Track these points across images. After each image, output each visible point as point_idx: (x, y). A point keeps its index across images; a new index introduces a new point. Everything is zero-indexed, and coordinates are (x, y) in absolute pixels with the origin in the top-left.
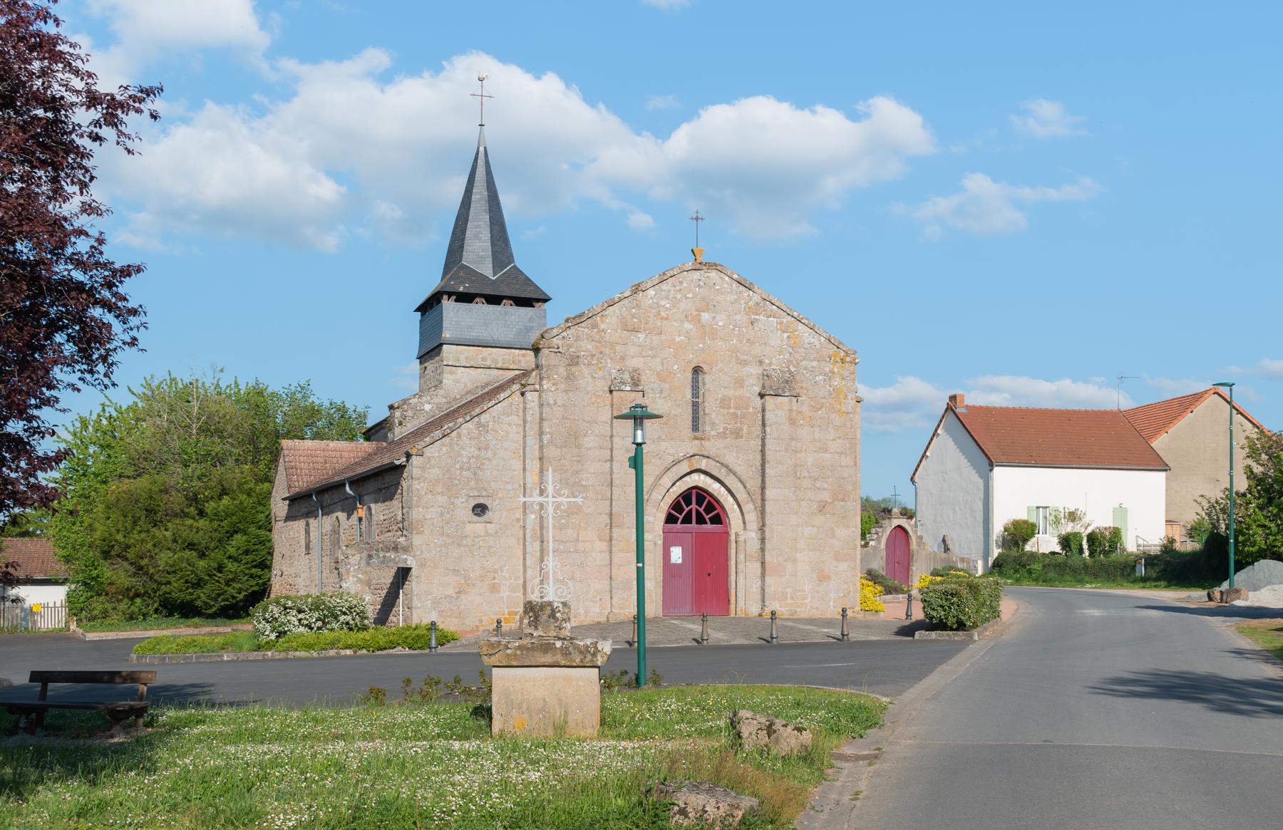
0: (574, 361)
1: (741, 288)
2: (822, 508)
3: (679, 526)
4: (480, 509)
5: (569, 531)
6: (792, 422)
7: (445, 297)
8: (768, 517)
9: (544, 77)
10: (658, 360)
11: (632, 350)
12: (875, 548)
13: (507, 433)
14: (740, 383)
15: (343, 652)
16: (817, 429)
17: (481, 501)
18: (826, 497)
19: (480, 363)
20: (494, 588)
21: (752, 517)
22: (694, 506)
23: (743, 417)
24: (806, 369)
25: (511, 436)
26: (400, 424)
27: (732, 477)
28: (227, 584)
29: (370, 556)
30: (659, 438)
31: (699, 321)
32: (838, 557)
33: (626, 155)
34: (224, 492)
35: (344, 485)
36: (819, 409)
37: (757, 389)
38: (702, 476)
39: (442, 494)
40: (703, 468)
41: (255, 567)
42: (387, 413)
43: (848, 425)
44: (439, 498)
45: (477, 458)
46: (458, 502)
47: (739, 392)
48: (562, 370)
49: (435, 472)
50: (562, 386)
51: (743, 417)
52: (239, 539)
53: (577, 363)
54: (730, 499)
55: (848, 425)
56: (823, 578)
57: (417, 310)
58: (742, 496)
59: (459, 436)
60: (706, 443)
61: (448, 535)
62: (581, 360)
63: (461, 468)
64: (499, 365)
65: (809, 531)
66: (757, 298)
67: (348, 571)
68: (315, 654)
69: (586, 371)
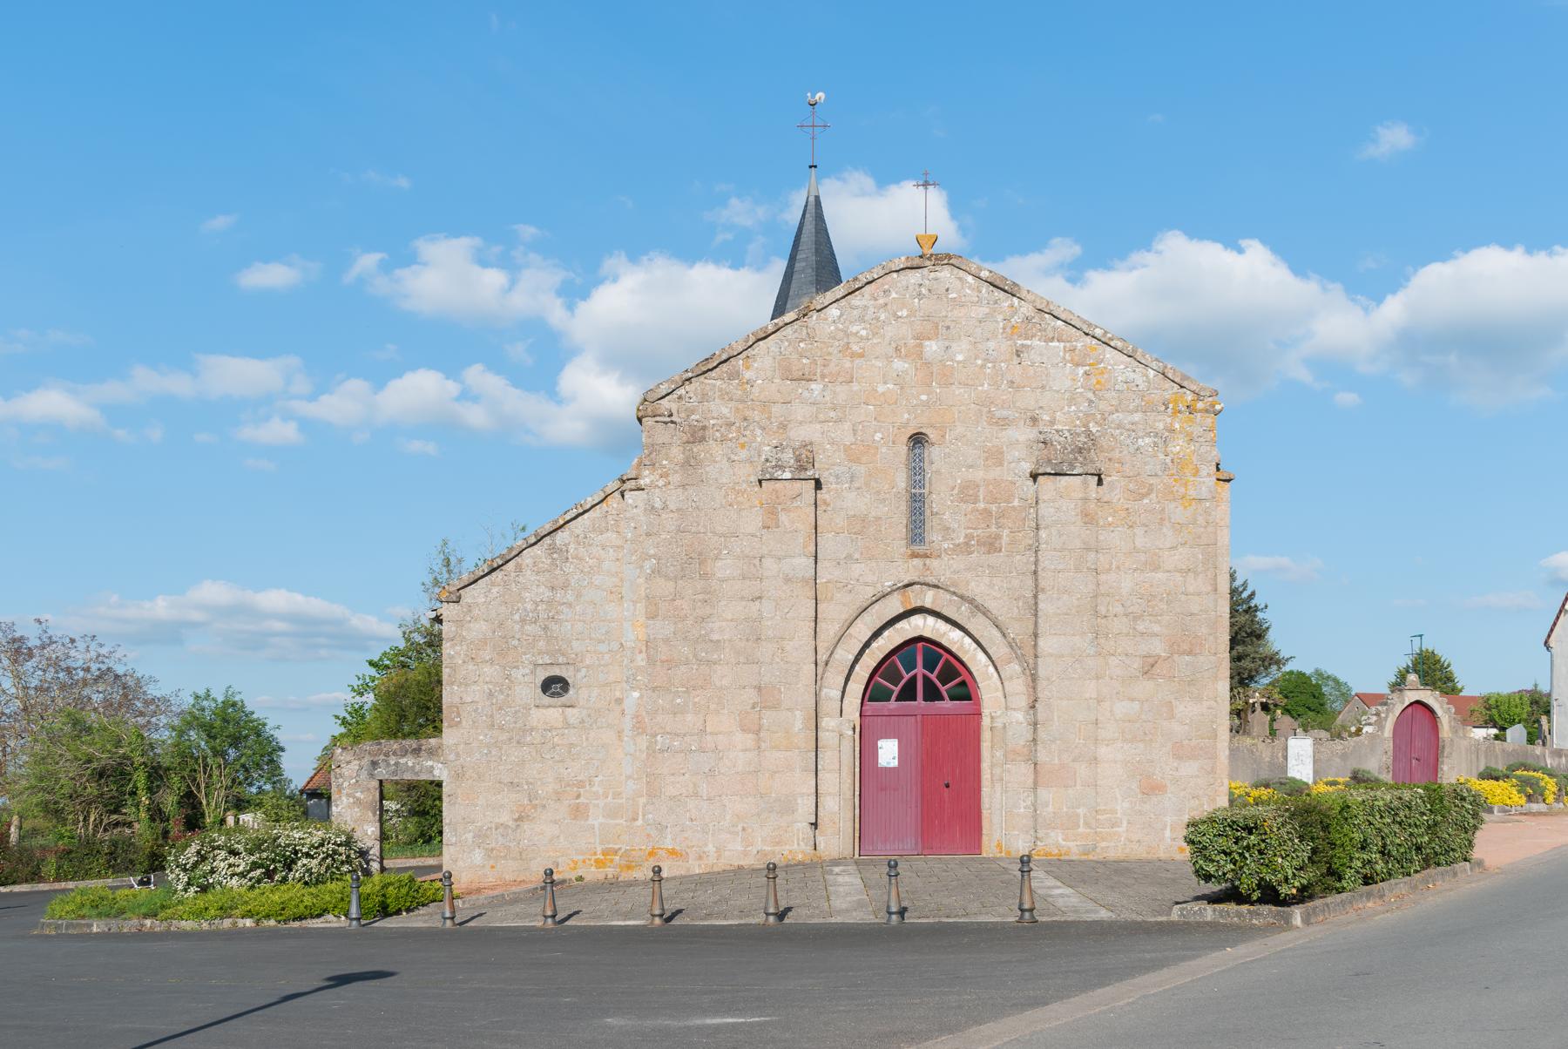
0: (698, 435)
1: (997, 293)
2: (1150, 667)
3: (893, 704)
4: (554, 685)
5: (689, 717)
6: (1088, 519)
8: (1042, 684)
10: (847, 426)
11: (800, 411)
12: (1372, 736)
13: (600, 561)
14: (995, 456)
15: (241, 923)
16: (1139, 531)
17: (556, 672)
18: (1158, 648)
20: (578, 812)
21: (1018, 686)
22: (920, 670)
23: (1002, 515)
24: (1119, 426)
25: (606, 565)
27: (980, 618)
29: (374, 764)
30: (849, 557)
31: (920, 355)
32: (1180, 753)
33: (1343, 325)
36: (1144, 496)
37: (1027, 467)
38: (931, 620)
39: (492, 662)
40: (928, 605)
43: (1201, 520)
44: (487, 669)
45: (550, 602)
46: (517, 674)
47: (995, 473)
48: (677, 453)
49: (478, 629)
50: (676, 478)
51: (1002, 515)
53: (703, 439)
54: (981, 656)
55: (1201, 520)
56: (1152, 789)
58: (999, 649)
59: (519, 569)
60: (934, 563)
61: (501, 728)
62: (708, 433)
63: (523, 621)
65: (1122, 708)
66: (1026, 309)
67: (340, 788)
68: (205, 925)
69: (717, 450)
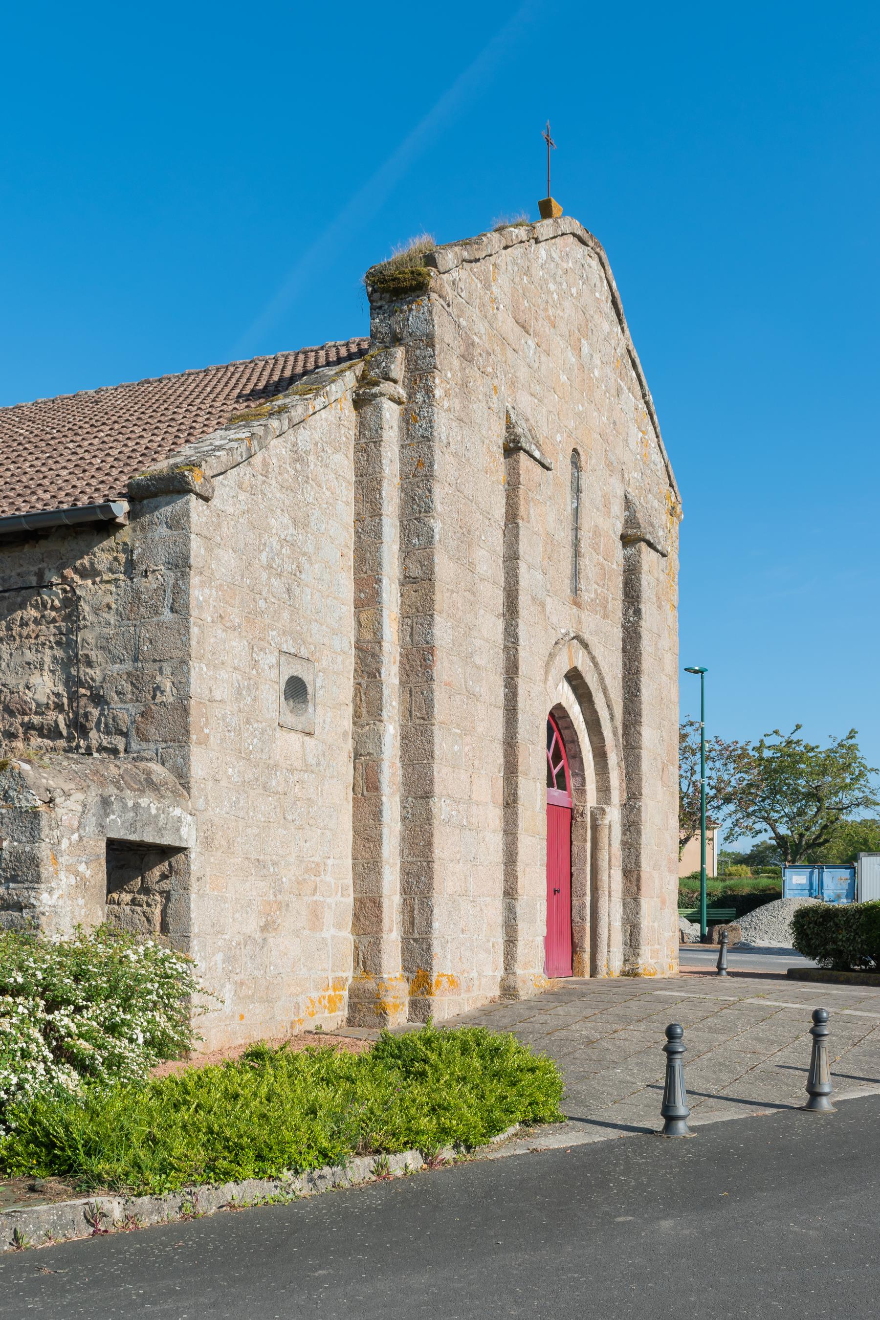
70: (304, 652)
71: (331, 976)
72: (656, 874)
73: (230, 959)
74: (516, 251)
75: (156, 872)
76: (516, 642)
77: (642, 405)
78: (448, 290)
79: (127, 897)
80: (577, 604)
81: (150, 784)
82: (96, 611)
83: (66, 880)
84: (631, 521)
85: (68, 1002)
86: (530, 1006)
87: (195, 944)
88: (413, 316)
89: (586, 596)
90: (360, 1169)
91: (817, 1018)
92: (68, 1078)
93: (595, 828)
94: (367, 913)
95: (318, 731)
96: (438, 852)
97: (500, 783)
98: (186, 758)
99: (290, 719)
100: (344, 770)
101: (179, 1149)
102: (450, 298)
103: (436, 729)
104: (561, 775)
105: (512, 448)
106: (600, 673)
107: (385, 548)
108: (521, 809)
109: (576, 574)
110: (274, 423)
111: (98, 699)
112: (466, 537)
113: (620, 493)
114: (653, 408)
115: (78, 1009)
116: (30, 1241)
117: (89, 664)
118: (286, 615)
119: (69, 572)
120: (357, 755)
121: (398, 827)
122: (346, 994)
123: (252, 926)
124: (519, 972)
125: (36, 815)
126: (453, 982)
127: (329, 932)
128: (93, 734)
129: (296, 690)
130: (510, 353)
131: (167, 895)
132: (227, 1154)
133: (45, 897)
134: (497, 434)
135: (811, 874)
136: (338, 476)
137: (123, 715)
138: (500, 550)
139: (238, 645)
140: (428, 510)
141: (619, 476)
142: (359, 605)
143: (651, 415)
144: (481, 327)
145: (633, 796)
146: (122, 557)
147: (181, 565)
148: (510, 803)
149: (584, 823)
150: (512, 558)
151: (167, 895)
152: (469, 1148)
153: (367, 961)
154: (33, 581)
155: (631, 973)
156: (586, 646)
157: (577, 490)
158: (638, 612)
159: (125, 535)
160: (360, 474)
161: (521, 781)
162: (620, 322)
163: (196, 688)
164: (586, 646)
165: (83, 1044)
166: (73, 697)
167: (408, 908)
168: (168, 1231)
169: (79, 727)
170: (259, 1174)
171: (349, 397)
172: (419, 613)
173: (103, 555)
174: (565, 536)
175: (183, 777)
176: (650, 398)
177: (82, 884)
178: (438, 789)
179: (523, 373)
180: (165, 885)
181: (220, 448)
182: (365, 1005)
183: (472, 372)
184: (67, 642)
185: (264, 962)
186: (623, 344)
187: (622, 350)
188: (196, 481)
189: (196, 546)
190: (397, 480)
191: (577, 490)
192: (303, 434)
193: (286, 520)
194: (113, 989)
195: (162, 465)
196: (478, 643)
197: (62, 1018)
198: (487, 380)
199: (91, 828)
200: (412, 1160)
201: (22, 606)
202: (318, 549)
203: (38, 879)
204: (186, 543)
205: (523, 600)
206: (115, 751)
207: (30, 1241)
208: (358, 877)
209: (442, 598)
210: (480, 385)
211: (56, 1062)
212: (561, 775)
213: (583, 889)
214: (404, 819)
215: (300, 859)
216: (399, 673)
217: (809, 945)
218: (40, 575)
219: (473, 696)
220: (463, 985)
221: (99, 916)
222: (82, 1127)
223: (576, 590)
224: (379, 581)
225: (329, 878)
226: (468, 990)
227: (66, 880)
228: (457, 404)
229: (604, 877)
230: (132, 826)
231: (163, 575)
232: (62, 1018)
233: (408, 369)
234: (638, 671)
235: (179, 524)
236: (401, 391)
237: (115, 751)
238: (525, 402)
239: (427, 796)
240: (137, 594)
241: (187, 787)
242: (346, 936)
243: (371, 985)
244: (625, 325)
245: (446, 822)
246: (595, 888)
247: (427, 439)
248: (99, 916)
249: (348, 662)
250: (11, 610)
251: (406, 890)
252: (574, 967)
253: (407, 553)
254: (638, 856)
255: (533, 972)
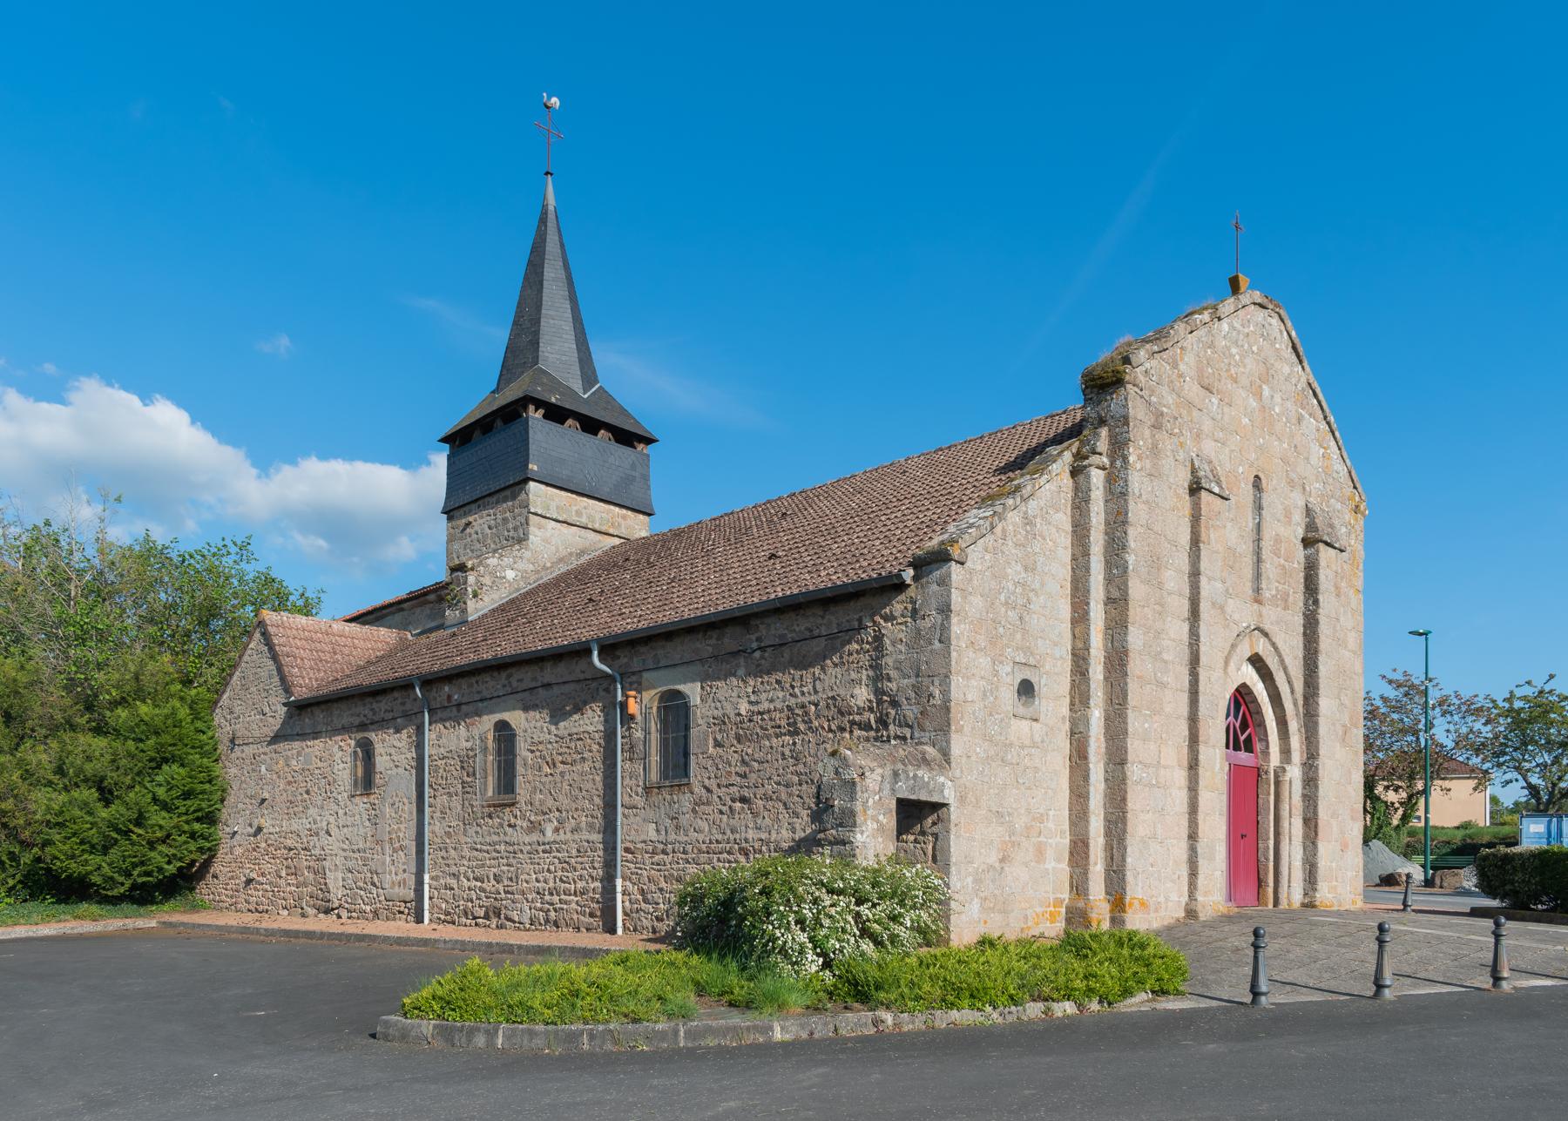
7: (531, 408)
9: (73, 397)
19: (574, 519)
26: (475, 595)
28: (152, 845)
34: (140, 694)
35: (589, 652)
41: (198, 820)
42: (442, 575)
52: (172, 770)
57: (444, 440)
64: (597, 526)
70: (1032, 661)
71: (1052, 897)
72: (1334, 822)
73: (977, 881)
74: (1201, 332)
75: (930, 821)
76: (1198, 640)
77: (1323, 426)
78: (1142, 379)
79: (911, 838)
80: (1258, 601)
81: (925, 761)
82: (893, 644)
83: (871, 826)
84: (1311, 526)
85: (868, 900)
86: (1205, 925)
87: (953, 869)
88: (1114, 404)
89: (1267, 594)
90: (1034, 1010)
91: (1381, 928)
92: (867, 946)
93: (1277, 783)
94: (1079, 851)
95: (1042, 718)
96: (1131, 804)
97: (1185, 750)
98: (948, 742)
99: (1021, 710)
100: (1063, 744)
101: (927, 987)
102: (1142, 385)
103: (1129, 712)
104: (1249, 741)
105: (1195, 489)
106: (1280, 656)
107: (1092, 579)
108: (1201, 771)
109: (1258, 576)
110: (1010, 502)
111: (895, 704)
112: (1156, 564)
113: (1302, 503)
114: (1334, 426)
115: (874, 905)
116: (843, 1032)
117: (889, 680)
118: (1018, 636)
119: (877, 618)
120: (1072, 733)
121: (1102, 786)
122: (1063, 910)
123: (993, 859)
124: (1200, 898)
125: (854, 784)
126: (1142, 904)
127: (1050, 864)
128: (891, 727)
129: (1026, 689)
130: (1195, 413)
131: (936, 836)
132: (955, 993)
133: (859, 836)
134: (1184, 478)
135: (1550, 823)
136: (1058, 529)
137: (910, 714)
138: (1186, 568)
139: (984, 661)
140: (1124, 547)
141: (1299, 489)
142: (1074, 622)
143: (1333, 432)
144: (1170, 399)
145: (1312, 755)
146: (910, 606)
147: (945, 610)
148: (1193, 766)
149: (1268, 780)
150: (1195, 574)
151: (936, 836)
152: (1110, 1004)
153: (1079, 886)
154: (856, 624)
155: (1309, 905)
156: (1266, 635)
157: (1259, 508)
158: (1316, 602)
159: (911, 592)
160: (1075, 525)
161: (1202, 748)
162: (1301, 362)
163: (955, 694)
164: (1266, 635)
165: (875, 926)
166: (880, 702)
167: (1109, 848)
168: (918, 1034)
169: (883, 722)
170: (972, 1007)
171: (1067, 470)
172: (1117, 625)
173: (898, 606)
174: (1246, 548)
175: (946, 754)
176: (1332, 419)
177: (881, 829)
178: (1130, 757)
179: (1207, 425)
180: (935, 829)
181: (971, 526)
182: (1077, 915)
183: (1162, 436)
184: (876, 666)
185: (1004, 880)
186: (1304, 380)
187: (1303, 384)
188: (955, 552)
189: (956, 597)
190: (1102, 527)
191: (1259, 508)
192: (1032, 503)
193: (1019, 568)
194: (894, 894)
195: (934, 543)
196: (1166, 643)
197: (864, 910)
198: (1175, 440)
199: (886, 792)
200: (1069, 1008)
201: (849, 642)
202: (1043, 585)
203: (854, 825)
204: (949, 596)
205: (1204, 606)
206: (904, 738)
207: (843, 1032)
208: (1072, 824)
209: (1135, 612)
210: (1167, 444)
211: (861, 937)
212: (1249, 741)
213: (1267, 834)
214: (1106, 780)
215: (1028, 811)
216: (1104, 673)
217: (1489, 886)
218: (860, 620)
219: (1162, 685)
220: (1152, 908)
221: (891, 848)
222: (874, 973)
223: (1258, 590)
224: (1088, 604)
225: (1051, 825)
226: (1156, 911)
227: (871, 826)
228: (1148, 464)
229: (1285, 824)
230: (912, 790)
231: (934, 617)
232: (864, 910)
233: (1111, 444)
234: (1316, 651)
235: (944, 582)
236: (1105, 460)
237: (904, 738)
238: (1209, 447)
239: (1122, 763)
240: (918, 631)
241: (948, 762)
242: (1064, 867)
243: (1081, 904)
244: (1306, 364)
245: (1138, 783)
246: (1277, 834)
247: (1124, 494)
248: (891, 849)
249: (1067, 665)
250: (843, 645)
251: (1108, 833)
252: (1260, 898)
253: (1109, 580)
254: (1316, 806)
255: (1214, 895)
